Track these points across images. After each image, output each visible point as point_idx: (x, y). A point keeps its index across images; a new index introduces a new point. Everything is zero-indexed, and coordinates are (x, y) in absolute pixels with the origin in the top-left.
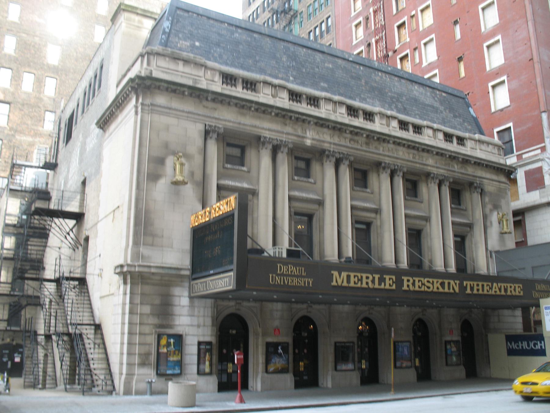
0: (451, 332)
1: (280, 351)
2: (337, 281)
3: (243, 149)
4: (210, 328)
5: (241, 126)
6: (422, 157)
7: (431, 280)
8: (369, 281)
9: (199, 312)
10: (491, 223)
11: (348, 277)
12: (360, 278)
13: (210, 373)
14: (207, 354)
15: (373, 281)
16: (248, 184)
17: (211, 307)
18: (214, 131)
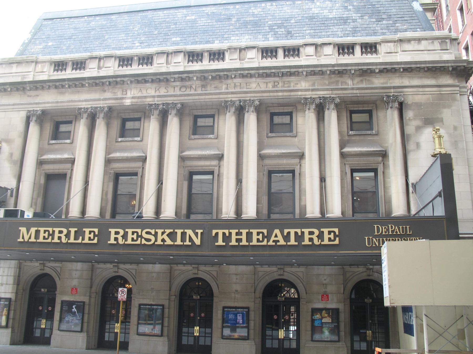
0: (325, 297)
1: (74, 310)
2: (23, 238)
3: (370, 113)
4: (11, 286)
5: (59, 104)
6: (289, 82)
7: (153, 232)
8: (314, 237)
9: (4, 272)
10: (418, 145)
11: (37, 232)
12: (51, 233)
13: (7, 327)
14: (5, 309)
15: (68, 236)
16: (69, 154)
17: (15, 268)
18: (33, 115)
